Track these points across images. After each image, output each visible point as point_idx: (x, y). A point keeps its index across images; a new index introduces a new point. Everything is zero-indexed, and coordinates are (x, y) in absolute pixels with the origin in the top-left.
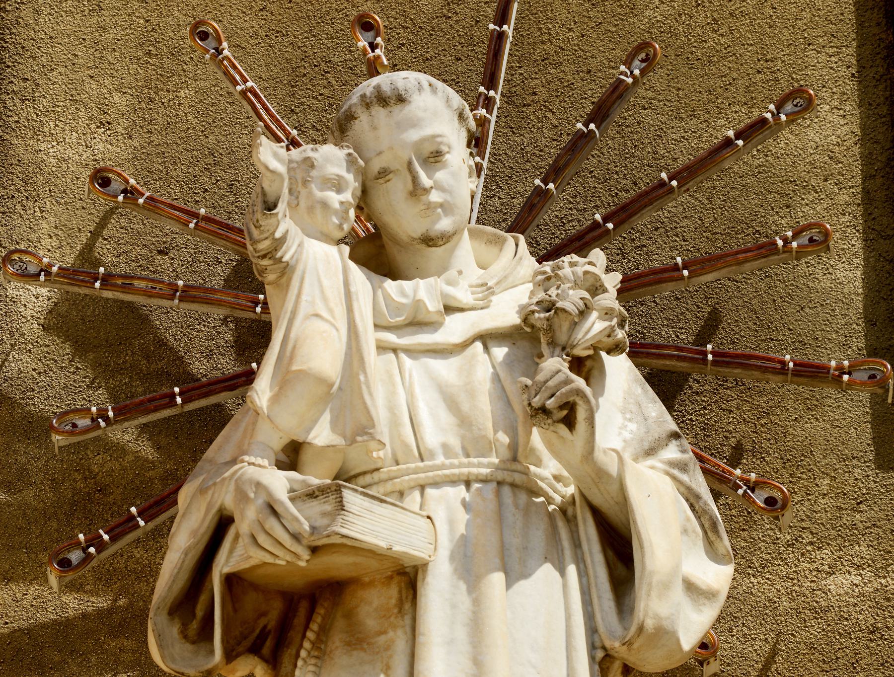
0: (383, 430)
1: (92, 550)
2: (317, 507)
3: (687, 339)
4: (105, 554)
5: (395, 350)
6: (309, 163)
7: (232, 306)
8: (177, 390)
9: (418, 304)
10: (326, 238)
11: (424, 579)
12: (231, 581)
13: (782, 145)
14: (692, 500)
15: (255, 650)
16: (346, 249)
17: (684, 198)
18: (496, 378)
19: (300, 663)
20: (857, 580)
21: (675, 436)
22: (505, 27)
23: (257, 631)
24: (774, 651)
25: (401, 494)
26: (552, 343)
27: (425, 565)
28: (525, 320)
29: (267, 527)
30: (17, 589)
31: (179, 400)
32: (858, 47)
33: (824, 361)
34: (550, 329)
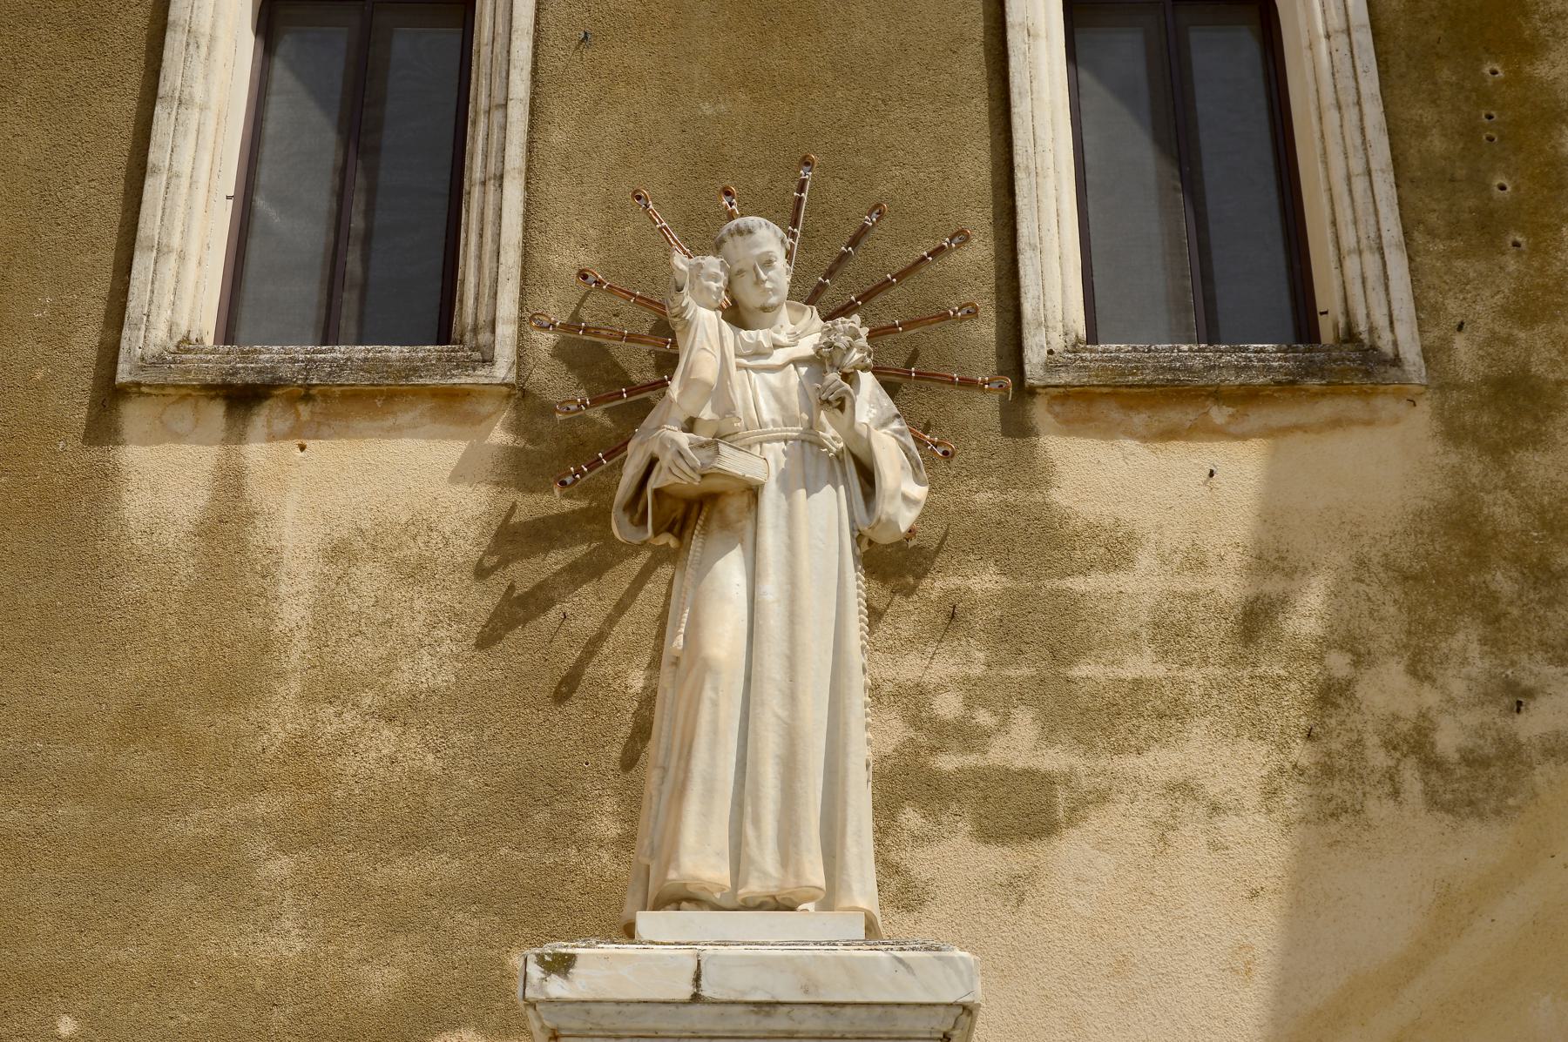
0: (740, 412)
1: (578, 476)
2: (704, 453)
3: (900, 365)
4: (585, 479)
5: (746, 368)
6: (700, 266)
7: (654, 345)
8: (624, 390)
9: (759, 343)
11: (762, 492)
13: (952, 260)
14: (907, 452)
15: (670, 530)
16: (720, 313)
17: (899, 289)
18: (801, 383)
19: (694, 537)
20: (991, 496)
21: (898, 416)
22: (803, 194)
23: (671, 520)
24: (946, 534)
25: (750, 447)
26: (832, 365)
27: (763, 485)
28: (817, 353)
29: (678, 464)
31: (625, 395)
32: (993, 208)
33: (974, 377)
34: (831, 357)
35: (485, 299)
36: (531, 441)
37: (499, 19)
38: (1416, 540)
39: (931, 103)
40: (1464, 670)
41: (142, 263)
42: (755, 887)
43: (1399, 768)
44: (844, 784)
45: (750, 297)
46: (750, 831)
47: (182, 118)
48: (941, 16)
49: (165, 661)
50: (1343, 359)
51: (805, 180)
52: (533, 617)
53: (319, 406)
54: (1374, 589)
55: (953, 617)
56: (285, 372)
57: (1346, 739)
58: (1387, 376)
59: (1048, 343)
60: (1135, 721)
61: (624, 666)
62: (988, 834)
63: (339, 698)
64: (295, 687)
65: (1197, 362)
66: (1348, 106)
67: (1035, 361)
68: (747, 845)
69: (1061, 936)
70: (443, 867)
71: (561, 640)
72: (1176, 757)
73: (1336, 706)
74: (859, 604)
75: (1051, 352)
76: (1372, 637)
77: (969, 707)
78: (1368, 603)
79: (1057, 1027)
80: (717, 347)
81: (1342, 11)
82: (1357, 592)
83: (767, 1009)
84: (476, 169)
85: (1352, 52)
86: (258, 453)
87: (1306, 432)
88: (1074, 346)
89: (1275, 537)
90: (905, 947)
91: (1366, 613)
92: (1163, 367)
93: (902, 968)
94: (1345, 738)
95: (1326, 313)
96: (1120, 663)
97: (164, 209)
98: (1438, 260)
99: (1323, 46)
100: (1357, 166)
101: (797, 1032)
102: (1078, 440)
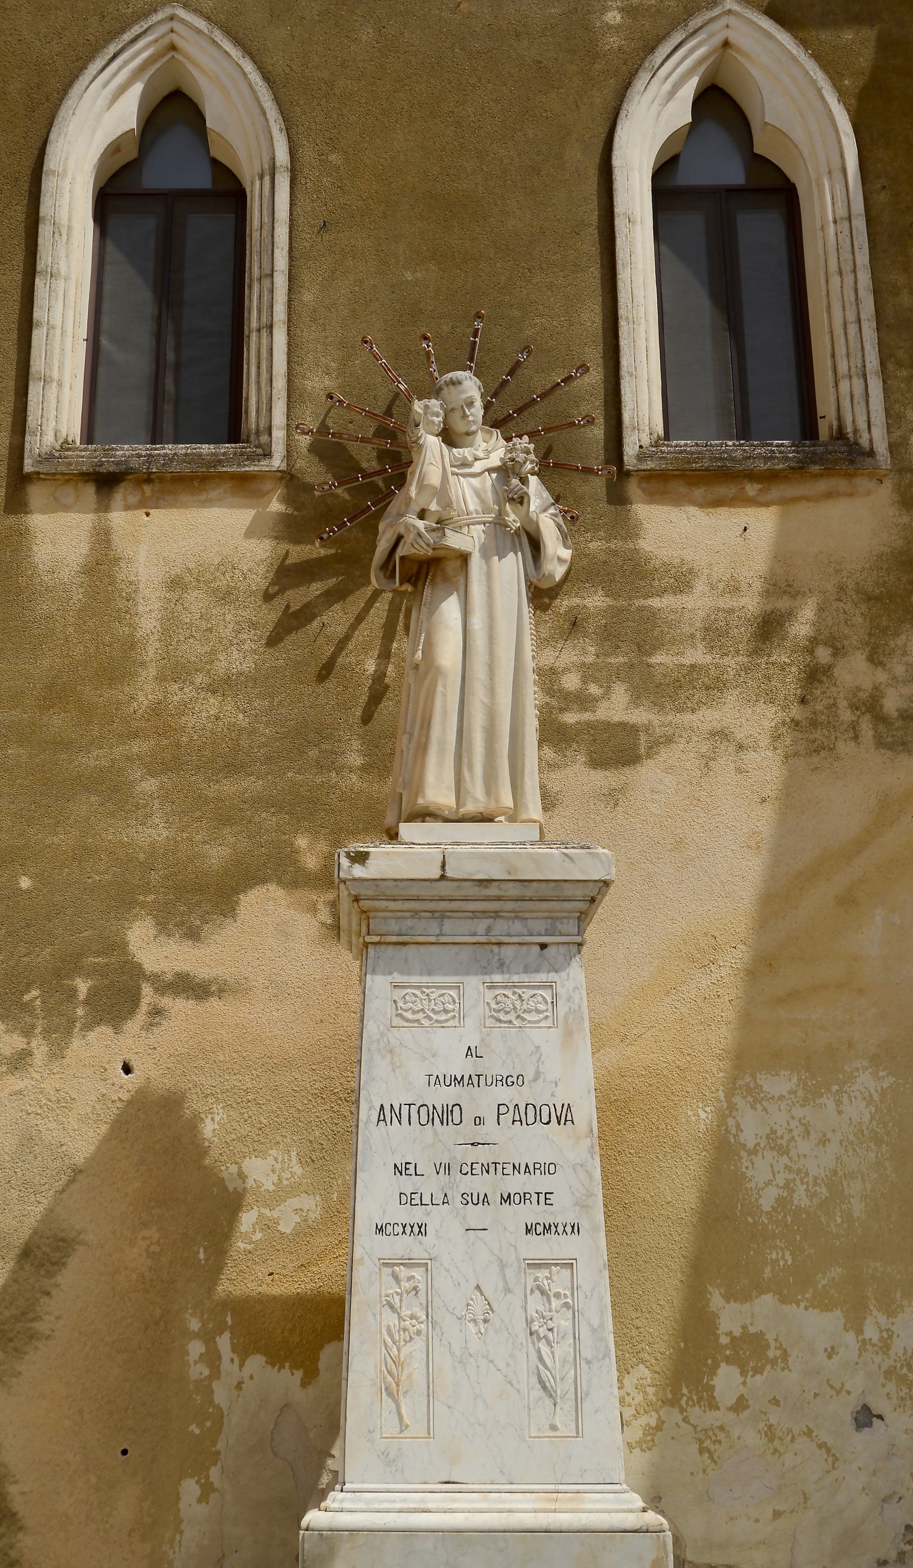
0: (455, 506)
2: (435, 534)
10: (432, 434)
12: (402, 558)
15: (409, 581)
18: (493, 485)
21: (553, 504)
25: (461, 527)
26: (513, 473)
30: (303, 546)
33: (591, 466)
35: (264, 412)
36: (297, 509)
37: (265, 212)
38: (878, 574)
39: (562, 271)
40: (904, 659)
41: (35, 390)
42: (470, 807)
43: (859, 721)
44: (523, 743)
45: (459, 426)
46: (466, 773)
47: (53, 286)
48: (568, 207)
49: (68, 656)
50: (836, 452)
51: (478, 329)
52: (304, 625)
53: (157, 486)
54: (848, 606)
55: (574, 624)
56: (134, 463)
57: (826, 703)
58: (864, 463)
59: (639, 440)
60: (691, 692)
61: (362, 657)
62: (596, 763)
63: (181, 678)
64: (153, 672)
65: (738, 454)
66: (847, 273)
67: (630, 454)
68: (465, 781)
69: (641, 826)
70: (251, 785)
71: (322, 640)
72: (717, 715)
73: (821, 682)
74: (531, 629)
75: (641, 447)
76: (846, 637)
77: (584, 682)
78: (844, 615)
79: (638, 881)
80: (440, 462)
81: (846, 204)
82: (838, 607)
83: (486, 883)
84: (253, 320)
85: (851, 234)
86: (118, 518)
87: (808, 501)
88: (656, 442)
89: (785, 571)
90: (568, 846)
91: (843, 622)
92: (715, 458)
93: (567, 860)
94: (825, 703)
95: (824, 417)
96: (682, 654)
97: (46, 351)
98: (902, 382)
99: (831, 228)
100: (851, 316)
101: (503, 897)
102: (658, 507)
